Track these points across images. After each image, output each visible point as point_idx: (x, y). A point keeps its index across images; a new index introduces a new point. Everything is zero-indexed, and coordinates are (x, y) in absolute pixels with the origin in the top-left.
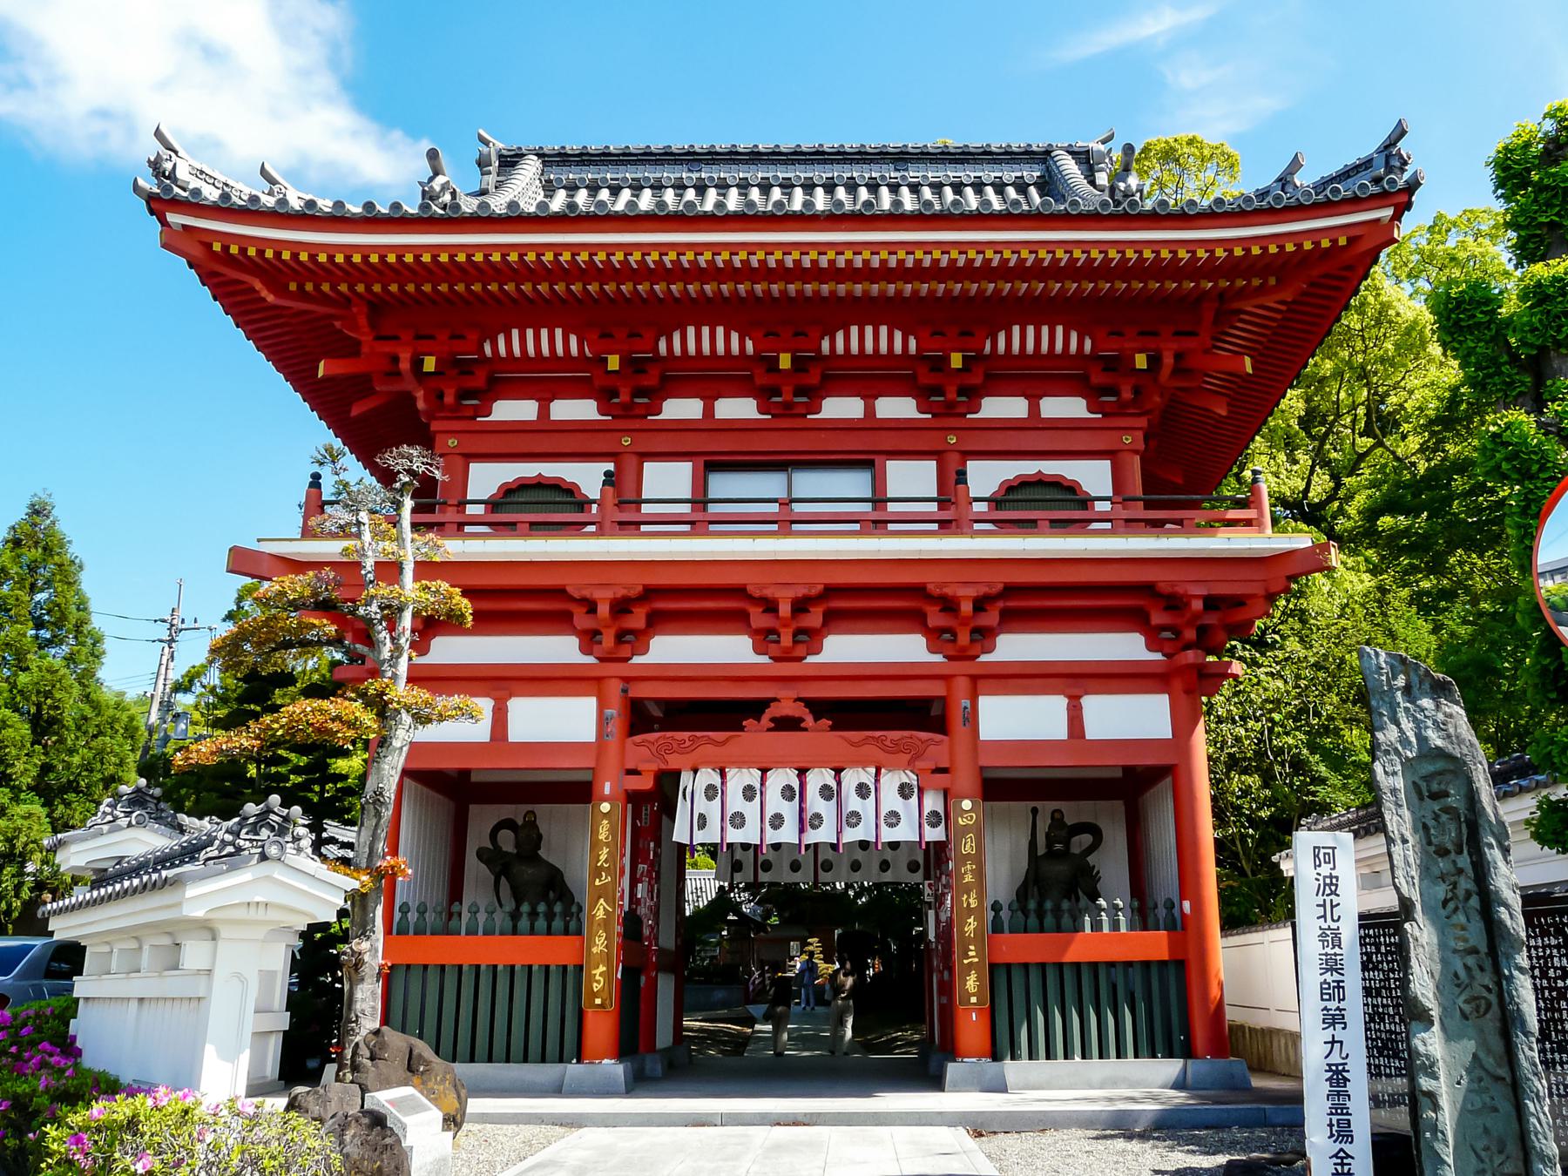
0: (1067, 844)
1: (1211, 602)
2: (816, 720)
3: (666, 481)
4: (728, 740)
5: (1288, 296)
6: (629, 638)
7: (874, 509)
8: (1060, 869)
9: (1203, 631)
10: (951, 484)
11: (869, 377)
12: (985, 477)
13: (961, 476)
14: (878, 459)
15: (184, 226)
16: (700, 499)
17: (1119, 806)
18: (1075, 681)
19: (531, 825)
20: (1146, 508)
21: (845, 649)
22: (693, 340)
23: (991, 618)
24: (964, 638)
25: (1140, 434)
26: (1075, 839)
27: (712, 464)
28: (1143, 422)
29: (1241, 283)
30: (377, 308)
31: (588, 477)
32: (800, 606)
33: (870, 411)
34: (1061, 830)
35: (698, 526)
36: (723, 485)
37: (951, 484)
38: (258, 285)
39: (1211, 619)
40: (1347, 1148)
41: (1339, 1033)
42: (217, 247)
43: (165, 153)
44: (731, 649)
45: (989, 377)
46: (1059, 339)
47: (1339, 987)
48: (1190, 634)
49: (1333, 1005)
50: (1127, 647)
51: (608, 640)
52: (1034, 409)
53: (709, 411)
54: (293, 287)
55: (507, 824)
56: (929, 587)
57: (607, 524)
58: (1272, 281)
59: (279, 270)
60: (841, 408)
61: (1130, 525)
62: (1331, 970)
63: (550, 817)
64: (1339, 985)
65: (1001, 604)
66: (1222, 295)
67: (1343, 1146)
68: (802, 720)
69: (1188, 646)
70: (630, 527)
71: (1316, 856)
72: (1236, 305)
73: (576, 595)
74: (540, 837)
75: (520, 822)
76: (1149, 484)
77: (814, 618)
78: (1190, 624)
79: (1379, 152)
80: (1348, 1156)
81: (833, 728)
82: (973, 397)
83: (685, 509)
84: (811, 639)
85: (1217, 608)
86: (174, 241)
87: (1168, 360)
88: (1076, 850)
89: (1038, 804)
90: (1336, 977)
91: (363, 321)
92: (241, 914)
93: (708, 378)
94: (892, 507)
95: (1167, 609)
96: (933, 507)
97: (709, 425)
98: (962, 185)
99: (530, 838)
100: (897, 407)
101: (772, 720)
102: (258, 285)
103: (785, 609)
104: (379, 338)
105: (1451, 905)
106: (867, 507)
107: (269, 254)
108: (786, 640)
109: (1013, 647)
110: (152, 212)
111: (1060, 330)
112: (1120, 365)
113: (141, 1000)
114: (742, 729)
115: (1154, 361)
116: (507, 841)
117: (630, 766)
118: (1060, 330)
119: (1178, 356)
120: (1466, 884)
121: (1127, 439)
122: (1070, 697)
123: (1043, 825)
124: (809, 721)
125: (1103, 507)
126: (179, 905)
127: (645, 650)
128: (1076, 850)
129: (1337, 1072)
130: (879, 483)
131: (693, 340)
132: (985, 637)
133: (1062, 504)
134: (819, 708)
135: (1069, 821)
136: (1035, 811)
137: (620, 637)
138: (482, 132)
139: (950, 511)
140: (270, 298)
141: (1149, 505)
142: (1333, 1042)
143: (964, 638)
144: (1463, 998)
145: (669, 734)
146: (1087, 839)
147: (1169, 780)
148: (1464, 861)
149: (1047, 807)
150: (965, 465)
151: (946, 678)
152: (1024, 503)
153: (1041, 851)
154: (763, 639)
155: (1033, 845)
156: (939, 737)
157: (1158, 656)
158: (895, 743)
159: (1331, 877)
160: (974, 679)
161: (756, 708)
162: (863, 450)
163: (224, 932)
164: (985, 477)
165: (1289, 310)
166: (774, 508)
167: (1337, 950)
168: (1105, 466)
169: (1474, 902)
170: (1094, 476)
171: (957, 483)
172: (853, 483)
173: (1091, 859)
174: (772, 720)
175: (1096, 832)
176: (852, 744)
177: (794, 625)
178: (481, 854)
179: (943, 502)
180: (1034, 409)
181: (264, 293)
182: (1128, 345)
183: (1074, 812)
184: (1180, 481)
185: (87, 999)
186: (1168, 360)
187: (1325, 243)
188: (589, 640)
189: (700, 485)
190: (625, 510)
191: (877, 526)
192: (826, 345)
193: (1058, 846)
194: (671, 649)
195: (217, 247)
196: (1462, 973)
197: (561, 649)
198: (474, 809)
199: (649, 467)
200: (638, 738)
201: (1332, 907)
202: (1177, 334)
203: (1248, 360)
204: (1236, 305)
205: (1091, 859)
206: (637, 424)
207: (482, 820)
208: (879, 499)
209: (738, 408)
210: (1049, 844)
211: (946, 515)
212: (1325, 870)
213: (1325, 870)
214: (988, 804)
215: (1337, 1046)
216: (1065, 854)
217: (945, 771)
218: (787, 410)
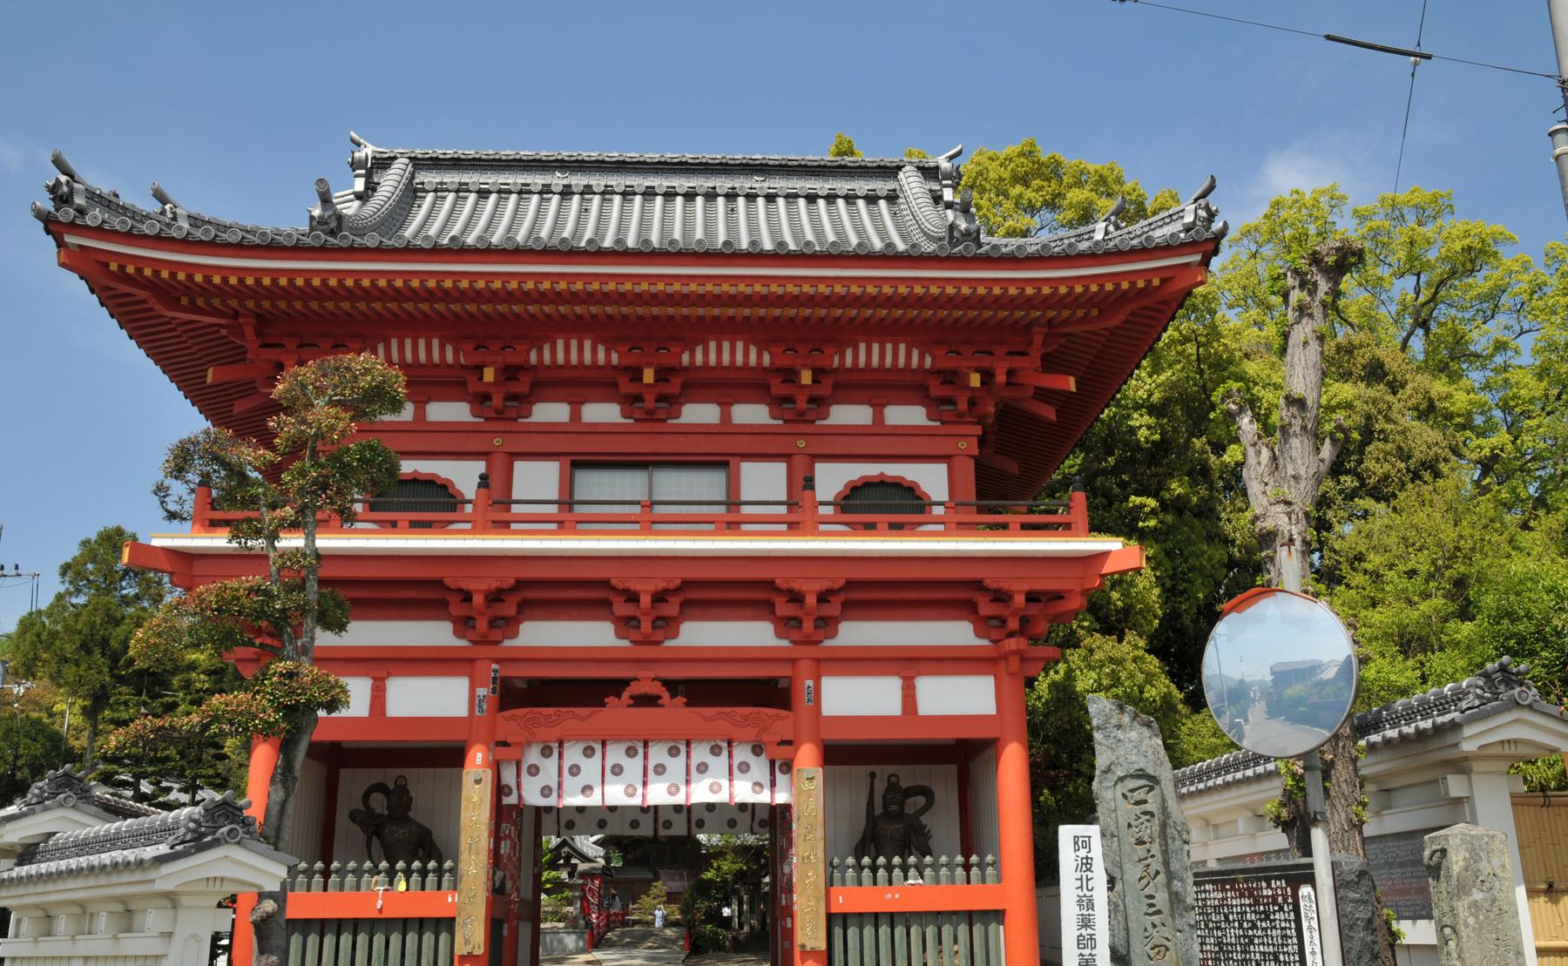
1: (1032, 597)
3: (536, 480)
4: (591, 715)
6: (500, 622)
7: (728, 511)
8: (893, 828)
9: (1025, 621)
10: (802, 483)
11: (726, 386)
12: (832, 479)
13: (809, 483)
14: (732, 461)
15: (81, 246)
16: (567, 501)
17: (953, 768)
18: (909, 664)
20: (979, 512)
21: (699, 634)
22: (563, 352)
23: (833, 609)
24: (808, 626)
25: (975, 441)
26: (911, 800)
27: (580, 462)
28: (978, 430)
29: (1066, 313)
30: (263, 321)
31: (464, 475)
32: (660, 597)
33: (726, 417)
35: (564, 526)
36: (592, 484)
37: (802, 483)
39: (1034, 609)
42: (114, 267)
43: (63, 178)
44: (593, 634)
45: (837, 386)
48: (1014, 624)
49: (1086, 952)
50: (957, 633)
51: (482, 625)
52: (878, 417)
53: (575, 415)
54: (184, 301)
55: (380, 788)
56: (778, 582)
58: (1095, 312)
59: (169, 290)
60: (699, 413)
61: (966, 529)
63: (420, 782)
64: (1092, 938)
65: (842, 597)
68: (659, 697)
69: (1011, 635)
70: (502, 526)
73: (453, 586)
74: (411, 799)
75: (391, 786)
77: (672, 608)
78: (1014, 614)
81: (687, 705)
82: (821, 403)
83: (553, 509)
84: (669, 625)
86: (75, 260)
87: (1001, 378)
88: (909, 810)
90: (1090, 931)
91: (249, 331)
92: (202, 887)
93: (577, 385)
94: (746, 510)
96: (783, 510)
98: (816, 197)
99: (400, 798)
100: (750, 414)
101: (632, 697)
103: (645, 600)
104: (264, 345)
105: (1144, 881)
106: (722, 509)
107: (165, 274)
108: (646, 626)
109: (855, 633)
110: (48, 232)
111: (902, 347)
112: (951, 377)
113: (86, 958)
114: (604, 705)
115: (987, 376)
116: (379, 803)
117: (500, 738)
118: (902, 347)
119: (1010, 373)
120: (1156, 864)
121: (963, 445)
122: (904, 678)
123: (880, 787)
124: (666, 695)
127: (515, 635)
128: (909, 810)
130: (733, 485)
131: (563, 352)
132: (828, 625)
133: (902, 504)
134: (672, 686)
135: (904, 784)
136: (873, 775)
137: (492, 624)
139: (798, 510)
141: (981, 510)
143: (808, 626)
145: (536, 710)
146: (921, 800)
148: (1156, 848)
149: (883, 771)
150: (812, 470)
151: (793, 661)
152: (862, 504)
153: (878, 811)
154: (625, 625)
155: (870, 804)
156: (783, 713)
157: (985, 642)
158: (745, 718)
160: (818, 661)
161: (616, 687)
162: (719, 454)
163: (185, 901)
164: (832, 479)
166: (637, 509)
168: (941, 469)
169: (1161, 878)
170: (932, 479)
171: (805, 488)
172: (709, 484)
173: (924, 819)
174: (632, 697)
175: (927, 793)
176: (705, 719)
177: (654, 614)
178: (353, 816)
179: (791, 504)
180: (878, 417)
182: (964, 363)
183: (909, 776)
185: (14, 959)
187: (1141, 284)
188: (463, 625)
189: (567, 485)
190: (498, 507)
191: (732, 526)
192: (685, 358)
193: (894, 808)
194: (541, 634)
195: (114, 267)
197: (436, 634)
198: (345, 774)
199: (519, 466)
200: (508, 713)
202: (1010, 353)
205: (924, 819)
206: (509, 426)
207: (354, 783)
208: (733, 501)
209: (602, 413)
210: (885, 806)
211: (794, 518)
212: (1083, 853)
213: (1083, 853)
214: (831, 768)
216: (900, 815)
217: (790, 743)
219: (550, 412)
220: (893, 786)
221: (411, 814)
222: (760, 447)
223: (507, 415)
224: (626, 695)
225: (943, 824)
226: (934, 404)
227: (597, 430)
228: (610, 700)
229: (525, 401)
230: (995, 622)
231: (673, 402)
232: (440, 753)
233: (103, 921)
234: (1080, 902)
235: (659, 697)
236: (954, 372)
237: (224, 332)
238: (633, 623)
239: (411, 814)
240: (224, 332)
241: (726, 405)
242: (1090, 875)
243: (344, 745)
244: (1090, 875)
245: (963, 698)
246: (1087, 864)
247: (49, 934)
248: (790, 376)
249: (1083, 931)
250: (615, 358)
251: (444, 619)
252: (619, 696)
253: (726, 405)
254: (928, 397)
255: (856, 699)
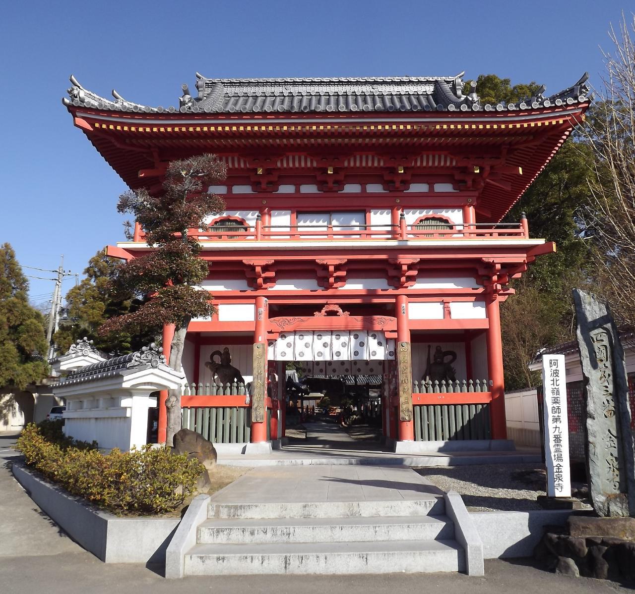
0: (442, 360)
2: (343, 312)
5: (537, 143)
17: (463, 344)
19: (227, 353)
25: (475, 198)
26: (445, 358)
28: (476, 194)
34: (440, 354)
38: (113, 140)
40: (561, 463)
41: (558, 424)
46: (445, 162)
47: (558, 409)
49: (556, 415)
54: (127, 141)
57: (259, 235)
58: (531, 137)
60: (352, 188)
62: (556, 403)
63: (235, 353)
66: (510, 144)
67: (559, 463)
68: (338, 312)
71: (551, 363)
72: (516, 147)
75: (222, 352)
76: (479, 218)
79: (576, 85)
80: (561, 466)
85: (506, 268)
89: (430, 344)
90: (558, 405)
95: (485, 268)
97: (298, 195)
100: (374, 188)
101: (326, 312)
102: (113, 140)
105: (603, 379)
110: (70, 111)
112: (466, 171)
113: (96, 419)
114: (314, 315)
116: (217, 359)
119: (492, 167)
123: (433, 352)
125: (458, 228)
126: (121, 383)
129: (557, 438)
135: (443, 350)
136: (429, 346)
138: (197, 73)
140: (118, 146)
141: (478, 227)
142: (556, 428)
144: (605, 411)
146: (450, 357)
147: (485, 334)
149: (434, 345)
153: (432, 362)
155: (429, 359)
159: (556, 370)
161: (319, 308)
165: (536, 152)
167: (558, 396)
173: (452, 365)
174: (326, 312)
175: (454, 355)
181: (116, 143)
183: (445, 347)
184: (490, 216)
185: (68, 419)
186: (488, 168)
193: (439, 360)
196: (606, 403)
201: (557, 381)
203: (520, 169)
204: (516, 147)
205: (452, 365)
207: (207, 352)
209: (309, 189)
210: (435, 359)
212: (554, 368)
213: (554, 368)
215: (557, 429)
218: (330, 190)
219: (286, 189)
220: (438, 350)
221: (231, 364)
222: (380, 203)
223: (268, 190)
224: (323, 311)
225: (460, 366)
226: (456, 183)
227: (307, 196)
228: (316, 313)
229: (275, 184)
230: (486, 278)
231: (340, 184)
232: (246, 339)
233: (101, 403)
234: (553, 392)
235: (338, 312)
236: (466, 168)
237: (145, 155)
238: (325, 280)
239: (231, 364)
240: (145, 155)
241: (363, 185)
242: (558, 378)
243: (202, 335)
244: (558, 378)
245: (468, 313)
246: (556, 373)
247: (81, 408)
248: (394, 171)
249: (555, 405)
250: (315, 165)
251: (244, 279)
252: (320, 312)
253: (363, 185)
254: (388, 275)
255: (422, 313)
